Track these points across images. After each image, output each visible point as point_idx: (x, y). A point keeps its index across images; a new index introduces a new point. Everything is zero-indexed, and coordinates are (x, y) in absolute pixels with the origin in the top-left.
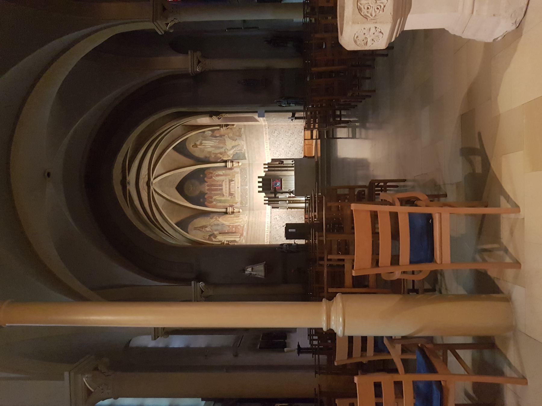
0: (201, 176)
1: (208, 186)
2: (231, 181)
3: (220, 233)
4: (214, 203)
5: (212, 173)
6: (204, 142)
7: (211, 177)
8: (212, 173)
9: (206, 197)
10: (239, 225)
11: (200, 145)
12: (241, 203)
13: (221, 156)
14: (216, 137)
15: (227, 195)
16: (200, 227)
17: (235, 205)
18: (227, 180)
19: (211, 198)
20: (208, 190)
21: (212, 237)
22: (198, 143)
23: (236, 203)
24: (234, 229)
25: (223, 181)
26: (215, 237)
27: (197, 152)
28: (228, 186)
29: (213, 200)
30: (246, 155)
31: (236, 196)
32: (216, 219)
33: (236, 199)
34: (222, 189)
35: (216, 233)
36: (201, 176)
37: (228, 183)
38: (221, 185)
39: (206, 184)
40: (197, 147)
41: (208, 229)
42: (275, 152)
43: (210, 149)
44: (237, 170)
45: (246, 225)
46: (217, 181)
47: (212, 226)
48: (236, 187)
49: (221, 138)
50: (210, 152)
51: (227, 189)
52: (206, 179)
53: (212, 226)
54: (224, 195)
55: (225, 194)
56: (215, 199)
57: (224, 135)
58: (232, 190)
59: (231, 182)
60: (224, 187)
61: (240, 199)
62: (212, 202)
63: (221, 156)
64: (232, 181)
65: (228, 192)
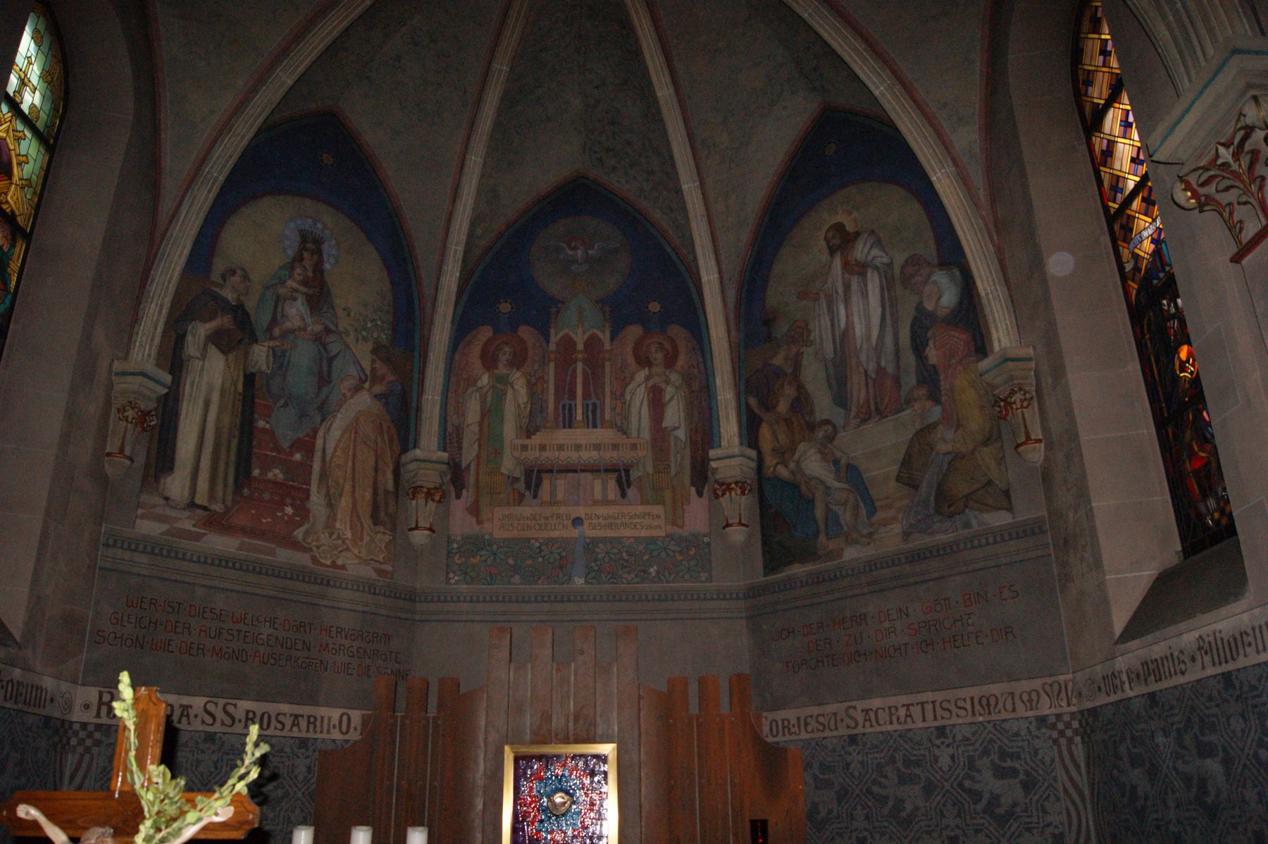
0: (655, 307)
1: (592, 343)
2: (623, 476)
3: (250, 379)
4: (485, 380)
5: (670, 362)
6: (874, 283)
7: (643, 361)
8: (670, 362)
9: (525, 332)
10: (303, 512)
11: (846, 265)
12: (476, 544)
13: (783, 407)
14: (919, 347)
15: (532, 455)
16: (318, 268)
17: (459, 507)
18: (626, 456)
19: (518, 361)
20: (568, 344)
21: (223, 321)
22: (861, 251)
23: (475, 510)
24: (276, 474)
25: (624, 431)
26: (218, 340)
27: (806, 253)
28: (589, 456)
29: (502, 369)
30: (797, 570)
31: (525, 510)
32: (375, 379)
33: (500, 512)
34: (569, 423)
35: (260, 355)
36: (655, 307)
37: (609, 456)
38: (593, 419)
39: (605, 336)
40: (832, 252)
41: (296, 311)
42: (587, 781)
43: (821, 329)
44: (697, 515)
45: (302, 559)
46: (619, 396)
47: (318, 339)
48: (580, 511)
49: (910, 380)
50: (801, 334)
51: (571, 456)
52: (634, 332)
53: (318, 339)
54: (529, 432)
55: (537, 439)
56: (504, 380)
57: (934, 397)
58: (562, 483)
59: (612, 484)
60: (581, 435)
61: (500, 534)
62: (489, 361)
63: (783, 407)
64: (624, 484)
65: (550, 456)
